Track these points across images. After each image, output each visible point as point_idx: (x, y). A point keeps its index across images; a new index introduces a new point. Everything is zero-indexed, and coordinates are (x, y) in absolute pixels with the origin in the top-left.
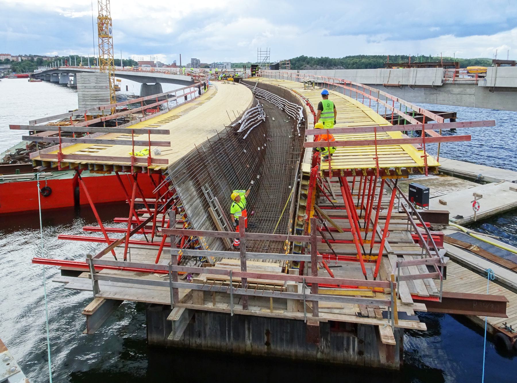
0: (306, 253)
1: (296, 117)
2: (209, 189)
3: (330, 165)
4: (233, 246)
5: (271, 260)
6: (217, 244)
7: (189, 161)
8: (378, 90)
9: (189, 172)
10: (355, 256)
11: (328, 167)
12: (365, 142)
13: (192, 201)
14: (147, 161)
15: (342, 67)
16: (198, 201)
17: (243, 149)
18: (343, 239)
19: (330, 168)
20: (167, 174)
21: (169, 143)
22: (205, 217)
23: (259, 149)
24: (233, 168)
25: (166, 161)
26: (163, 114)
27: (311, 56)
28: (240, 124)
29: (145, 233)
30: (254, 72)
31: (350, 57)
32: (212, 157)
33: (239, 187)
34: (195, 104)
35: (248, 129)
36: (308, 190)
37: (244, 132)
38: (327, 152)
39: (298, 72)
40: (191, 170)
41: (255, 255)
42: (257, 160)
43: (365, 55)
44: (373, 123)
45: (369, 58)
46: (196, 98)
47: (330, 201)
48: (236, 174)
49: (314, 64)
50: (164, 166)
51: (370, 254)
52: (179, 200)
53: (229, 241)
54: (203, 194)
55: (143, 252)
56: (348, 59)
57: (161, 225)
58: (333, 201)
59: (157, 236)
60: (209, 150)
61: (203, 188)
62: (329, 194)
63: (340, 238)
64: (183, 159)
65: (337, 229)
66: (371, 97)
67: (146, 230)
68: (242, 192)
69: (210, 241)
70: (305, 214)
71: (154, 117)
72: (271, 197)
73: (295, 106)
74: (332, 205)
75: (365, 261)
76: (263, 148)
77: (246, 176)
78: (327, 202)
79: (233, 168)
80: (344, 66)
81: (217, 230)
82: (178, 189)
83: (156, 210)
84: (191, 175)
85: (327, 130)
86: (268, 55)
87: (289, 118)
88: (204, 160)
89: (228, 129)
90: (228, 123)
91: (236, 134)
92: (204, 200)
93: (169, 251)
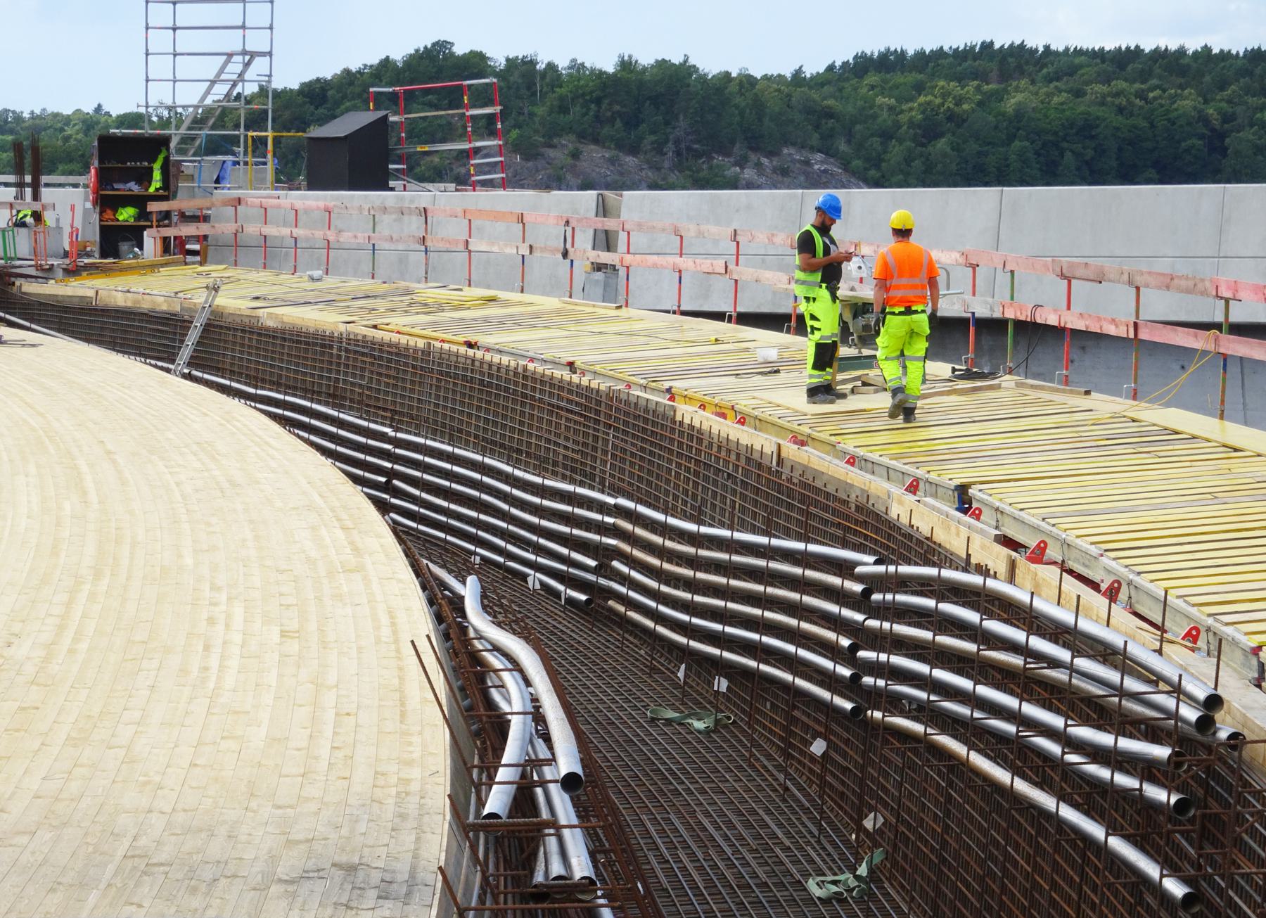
15: (818, 162)
27: (518, 52)
30: (126, 214)
31: (890, 63)
39: (604, 209)
43: (1036, 42)
45: (1072, 71)
49: (552, 133)
56: (872, 78)
73: (845, 568)
80: (843, 146)
86: (257, 42)
87: (722, 684)
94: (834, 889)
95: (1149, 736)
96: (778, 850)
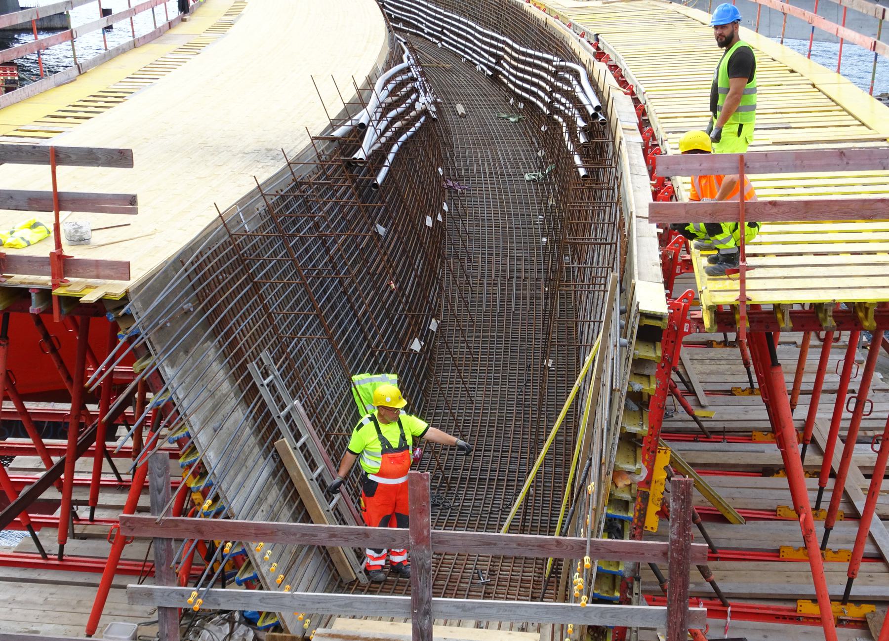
0: (634, 599)
1: (549, 106)
2: (275, 373)
3: (743, 290)
4: (367, 571)
5: (508, 624)
6: (310, 567)
7: (200, 267)
8: (880, 7)
9: (204, 311)
10: (790, 606)
11: (738, 294)
12: (880, 205)
13: (219, 417)
14: (49, 269)
16: (239, 415)
17: (372, 224)
18: (744, 544)
19: (743, 298)
20: (128, 316)
21: (132, 200)
22: (265, 474)
23: (429, 222)
24: (345, 292)
25: (122, 269)
26: (59, 85)
28: (361, 129)
29: (32, 527)
32: (275, 253)
33: (368, 362)
34: (175, 47)
35: (387, 146)
36: (653, 379)
37: (378, 157)
38: (727, 240)
40: (210, 303)
41: (463, 607)
42: (419, 263)
44: (862, 132)
46: (170, 25)
47: (690, 412)
48: (355, 315)
50: (116, 288)
51: (845, 599)
52: (178, 412)
53: (352, 556)
54: (254, 389)
55: (31, 592)
57: (87, 498)
58: (698, 412)
59: (75, 536)
60: (264, 227)
61: (253, 367)
62: (684, 387)
63: (734, 544)
64: (179, 261)
65: (722, 511)
66: (848, 33)
67: (35, 517)
68: (387, 380)
69: (287, 558)
70: (640, 465)
71: (29, 97)
72: (478, 396)
74: (695, 425)
75: (840, 622)
76: (440, 218)
77: (390, 323)
78: (676, 417)
79: (345, 292)
81: (307, 518)
82: (169, 372)
83: (73, 443)
84: (209, 321)
85: (742, 156)
87: (521, 105)
88: (249, 266)
89: (322, 146)
90: (319, 126)
91: (352, 165)
92: (260, 411)
93: (149, 594)
94: (533, 177)
95: (877, 314)
96: (520, 164)
